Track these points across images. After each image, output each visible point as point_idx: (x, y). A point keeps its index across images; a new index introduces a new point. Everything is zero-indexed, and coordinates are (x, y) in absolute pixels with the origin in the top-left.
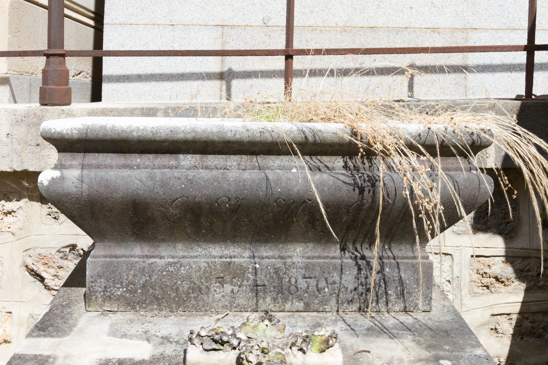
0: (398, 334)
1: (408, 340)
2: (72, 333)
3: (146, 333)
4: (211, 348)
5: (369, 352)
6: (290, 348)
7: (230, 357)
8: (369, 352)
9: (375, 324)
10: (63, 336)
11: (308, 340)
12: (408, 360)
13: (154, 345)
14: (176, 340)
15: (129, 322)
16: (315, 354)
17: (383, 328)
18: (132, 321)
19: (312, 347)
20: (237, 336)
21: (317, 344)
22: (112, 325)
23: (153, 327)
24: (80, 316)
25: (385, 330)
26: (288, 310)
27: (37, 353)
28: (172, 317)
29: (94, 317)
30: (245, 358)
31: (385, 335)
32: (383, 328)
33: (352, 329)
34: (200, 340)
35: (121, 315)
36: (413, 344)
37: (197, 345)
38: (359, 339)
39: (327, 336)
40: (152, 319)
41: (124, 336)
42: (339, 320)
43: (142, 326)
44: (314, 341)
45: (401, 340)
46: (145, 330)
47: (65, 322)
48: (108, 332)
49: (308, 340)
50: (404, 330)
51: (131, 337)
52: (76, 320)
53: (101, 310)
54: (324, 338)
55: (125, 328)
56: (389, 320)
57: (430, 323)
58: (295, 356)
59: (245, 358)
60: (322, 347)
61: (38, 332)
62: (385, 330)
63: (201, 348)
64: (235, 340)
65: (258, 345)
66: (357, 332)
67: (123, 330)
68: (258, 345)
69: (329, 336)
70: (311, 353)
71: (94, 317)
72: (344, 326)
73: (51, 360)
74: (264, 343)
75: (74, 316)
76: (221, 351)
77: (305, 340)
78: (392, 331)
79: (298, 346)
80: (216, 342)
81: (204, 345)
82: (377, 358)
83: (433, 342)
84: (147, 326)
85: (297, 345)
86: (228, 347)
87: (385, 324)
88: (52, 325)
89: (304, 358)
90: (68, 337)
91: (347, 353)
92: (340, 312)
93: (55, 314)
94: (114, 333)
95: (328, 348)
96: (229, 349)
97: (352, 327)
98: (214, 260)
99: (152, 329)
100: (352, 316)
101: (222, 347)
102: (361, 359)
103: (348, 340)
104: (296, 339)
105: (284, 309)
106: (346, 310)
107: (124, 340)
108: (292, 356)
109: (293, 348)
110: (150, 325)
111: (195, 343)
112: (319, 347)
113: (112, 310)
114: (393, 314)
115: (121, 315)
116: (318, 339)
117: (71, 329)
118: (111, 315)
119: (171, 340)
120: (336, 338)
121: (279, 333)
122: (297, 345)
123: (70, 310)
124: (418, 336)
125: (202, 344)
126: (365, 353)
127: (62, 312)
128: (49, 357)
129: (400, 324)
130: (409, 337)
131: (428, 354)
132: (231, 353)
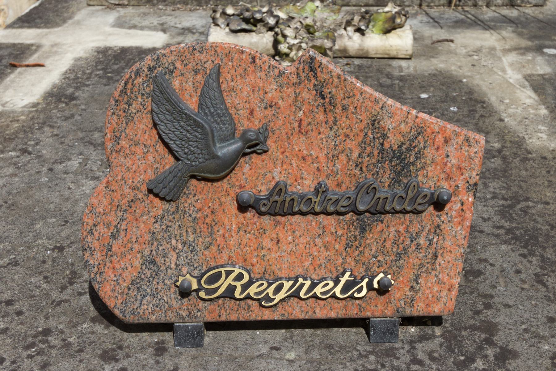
0: (495, 26)
1: (508, 33)
2: (66, 25)
3: (162, 24)
4: (239, 28)
5: (452, 41)
6: (345, 29)
7: (265, 40)
8: (452, 41)
9: (468, 18)
10: (53, 27)
11: (367, 16)
12: (502, 48)
13: (171, 35)
14: (200, 31)
15: (142, 15)
16: (377, 35)
17: (477, 20)
18: (145, 14)
19: (373, 26)
20: (275, 13)
21: (381, 23)
22: (119, 18)
23: (173, 19)
24: (79, 10)
25: (479, 23)
26: (354, 3)
27: (16, 41)
28: (199, 11)
29: (98, 11)
30: (279, 32)
31: (478, 27)
32: (477, 20)
33: (436, 22)
34: (226, 20)
35: (133, 9)
36: (512, 35)
37: (223, 26)
38: (443, 31)
39: (393, 13)
40: (173, 13)
41: (134, 27)
42: (421, 14)
43: (159, 19)
44: (376, 20)
45: (497, 31)
46: (161, 22)
47: (57, 15)
48: (114, 24)
49: (367, 16)
50: (504, 22)
51: (142, 28)
52: (73, 13)
53: (107, 4)
54: (389, 15)
55: (136, 21)
56: (486, 14)
57: (541, 16)
58: (350, 38)
59: (279, 32)
60: (387, 26)
61: (20, 24)
62: (479, 23)
63: (227, 30)
64: (272, 19)
65: (301, 22)
66: (441, 25)
67: (132, 22)
68: (301, 22)
69: (396, 13)
70: (372, 35)
71: (98, 11)
72: (425, 19)
73: (34, 48)
74: (308, 19)
75: (71, 10)
76: (254, 34)
77: (363, 17)
78: (489, 23)
79: (355, 25)
80: (246, 21)
81: (230, 25)
82: (461, 46)
83: (540, 33)
84: (164, 19)
85: (353, 23)
86: (262, 28)
87: (481, 17)
88: (40, 18)
89: (362, 41)
90: (60, 28)
91: (423, 42)
92: (423, 7)
93: (46, 8)
94: (120, 24)
95: (394, 29)
96: (264, 30)
97: (436, 20)
98: (427, 230)
99: (171, 21)
100: (438, 10)
101: (254, 28)
102: (440, 48)
103: (428, 32)
104: (352, 16)
105: (348, 3)
106: (432, 4)
107: (132, 31)
108: (347, 38)
109: (349, 29)
110: (170, 18)
111: (219, 23)
112: (382, 26)
113: (121, 2)
114: (494, 8)
115: (133, 9)
116: (382, 17)
117: (64, 21)
118: (120, 9)
119: (195, 31)
120: (405, 15)
121: (332, 14)
122: (353, 23)
123: (66, 5)
124: (522, 28)
125: (228, 25)
126: (446, 43)
127: (56, 6)
128: (32, 45)
129: (503, 17)
130: (509, 28)
131: (530, 43)
132: (266, 35)
